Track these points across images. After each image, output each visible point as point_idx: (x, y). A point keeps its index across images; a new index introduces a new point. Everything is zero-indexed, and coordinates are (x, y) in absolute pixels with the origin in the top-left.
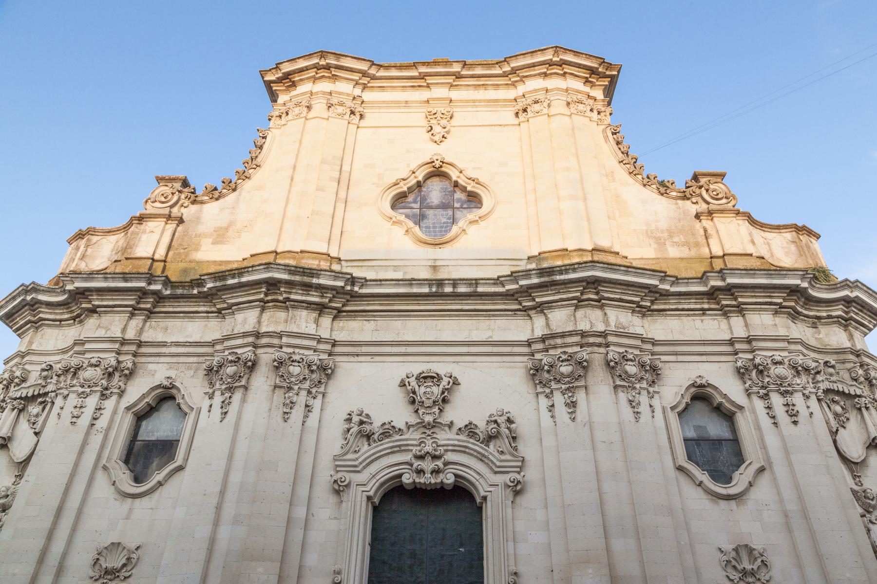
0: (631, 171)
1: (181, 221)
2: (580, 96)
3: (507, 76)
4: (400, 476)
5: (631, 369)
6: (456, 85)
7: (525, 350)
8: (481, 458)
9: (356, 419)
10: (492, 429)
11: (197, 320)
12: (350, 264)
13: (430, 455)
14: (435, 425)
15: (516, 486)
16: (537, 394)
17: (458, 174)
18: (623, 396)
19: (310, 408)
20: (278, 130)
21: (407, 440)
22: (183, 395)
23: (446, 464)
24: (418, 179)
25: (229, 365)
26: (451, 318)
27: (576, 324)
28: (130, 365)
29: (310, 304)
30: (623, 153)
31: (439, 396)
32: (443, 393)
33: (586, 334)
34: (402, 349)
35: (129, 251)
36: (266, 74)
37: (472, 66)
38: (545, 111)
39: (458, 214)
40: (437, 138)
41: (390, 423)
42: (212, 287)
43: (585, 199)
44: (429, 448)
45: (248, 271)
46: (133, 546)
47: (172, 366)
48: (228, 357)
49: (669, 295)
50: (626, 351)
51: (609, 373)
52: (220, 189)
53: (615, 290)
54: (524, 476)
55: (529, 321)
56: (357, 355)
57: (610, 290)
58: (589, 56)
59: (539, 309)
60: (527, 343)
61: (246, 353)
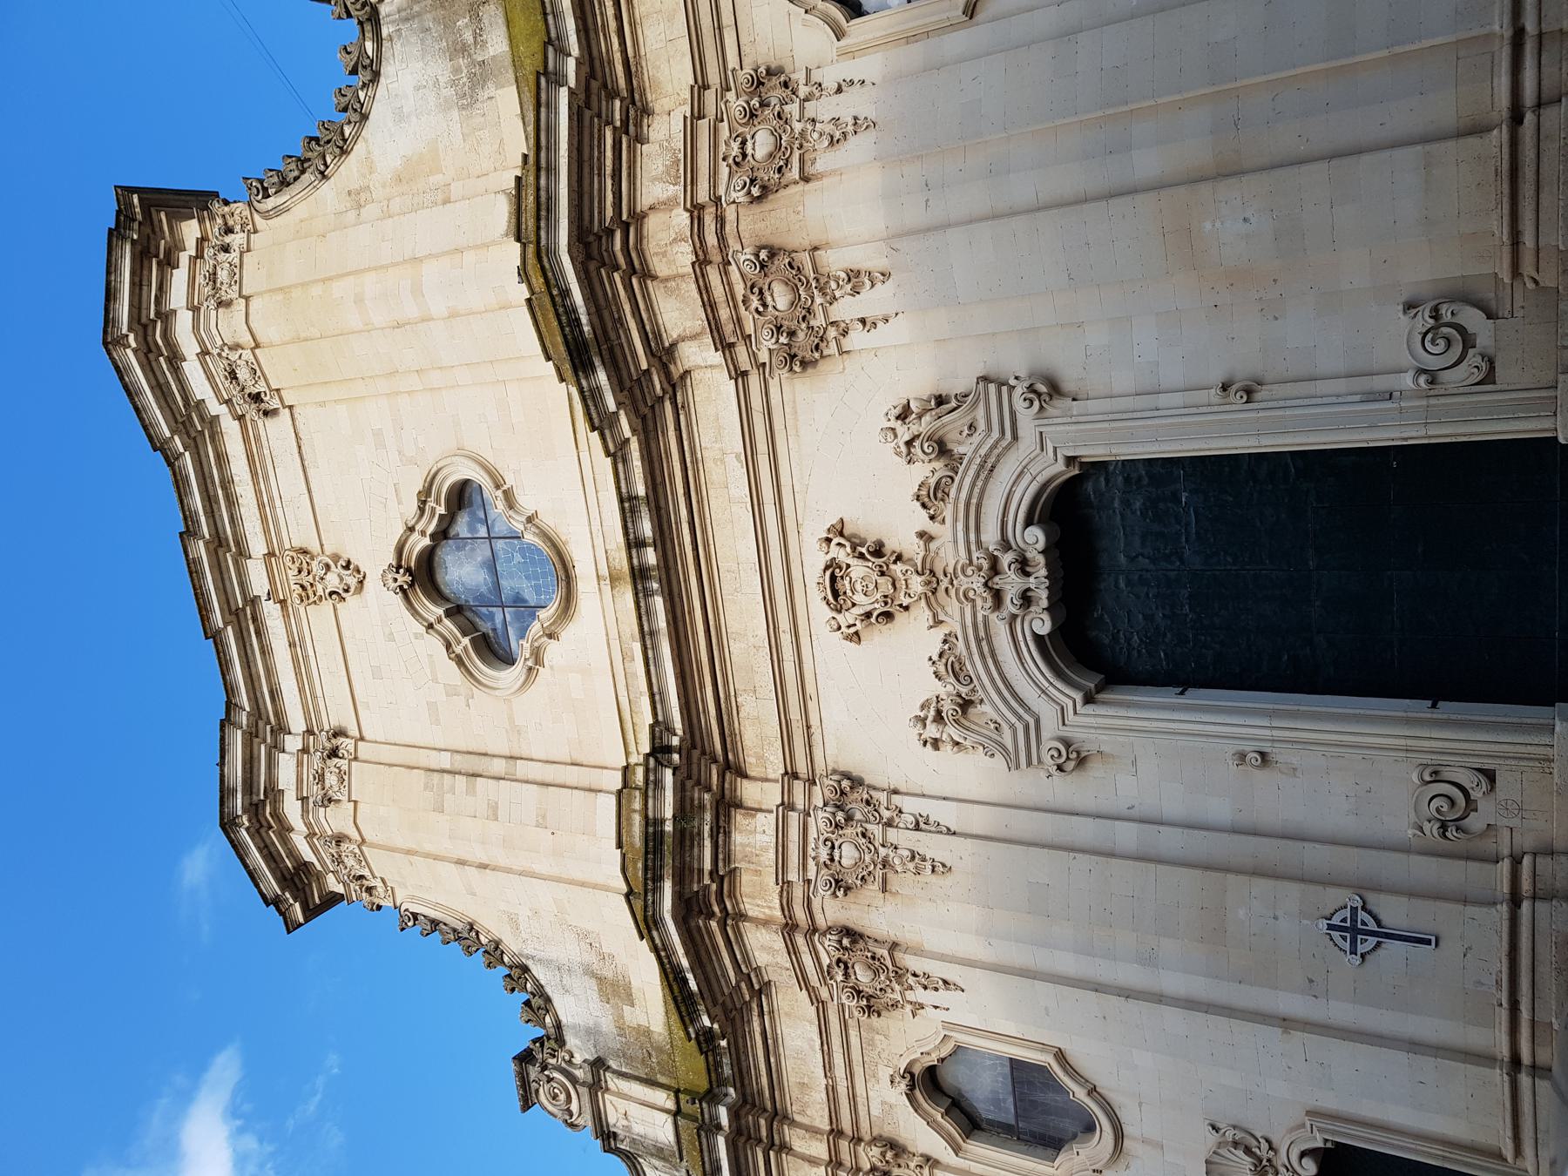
0: (337, 151)
1: (598, 1065)
2: (200, 280)
3: (194, 439)
4: (1038, 639)
5: (762, 145)
6: (237, 544)
7: (754, 381)
8: (988, 469)
9: (932, 731)
10: (924, 452)
11: (779, 1032)
12: (632, 748)
13: (990, 578)
14: (928, 571)
15: (1039, 395)
16: (841, 352)
17: (415, 536)
18: (824, 160)
19: (920, 819)
20: (396, 891)
21: (964, 627)
22: (922, 1054)
23: (1006, 545)
24: (443, 616)
25: (853, 977)
26: (711, 542)
27: (683, 276)
28: (875, 1151)
29: (718, 827)
30: (303, 172)
31: (870, 564)
32: (861, 556)
33: (700, 253)
34: (786, 639)
35: (666, 1153)
36: (292, 921)
37: (189, 517)
38: (247, 355)
39: (499, 529)
40: (352, 582)
41: (934, 663)
42: (709, 1017)
43: (416, 260)
44: (977, 583)
45: (668, 957)
46: (1213, 1138)
47: (871, 1073)
48: (838, 981)
49: (590, 54)
50: (724, 159)
51: (779, 195)
52: (525, 996)
53: (596, 193)
54: (1016, 378)
55: (695, 375)
56: (808, 727)
57: (596, 204)
58: (111, 268)
59: (664, 358)
60: (740, 380)
61: (827, 949)
